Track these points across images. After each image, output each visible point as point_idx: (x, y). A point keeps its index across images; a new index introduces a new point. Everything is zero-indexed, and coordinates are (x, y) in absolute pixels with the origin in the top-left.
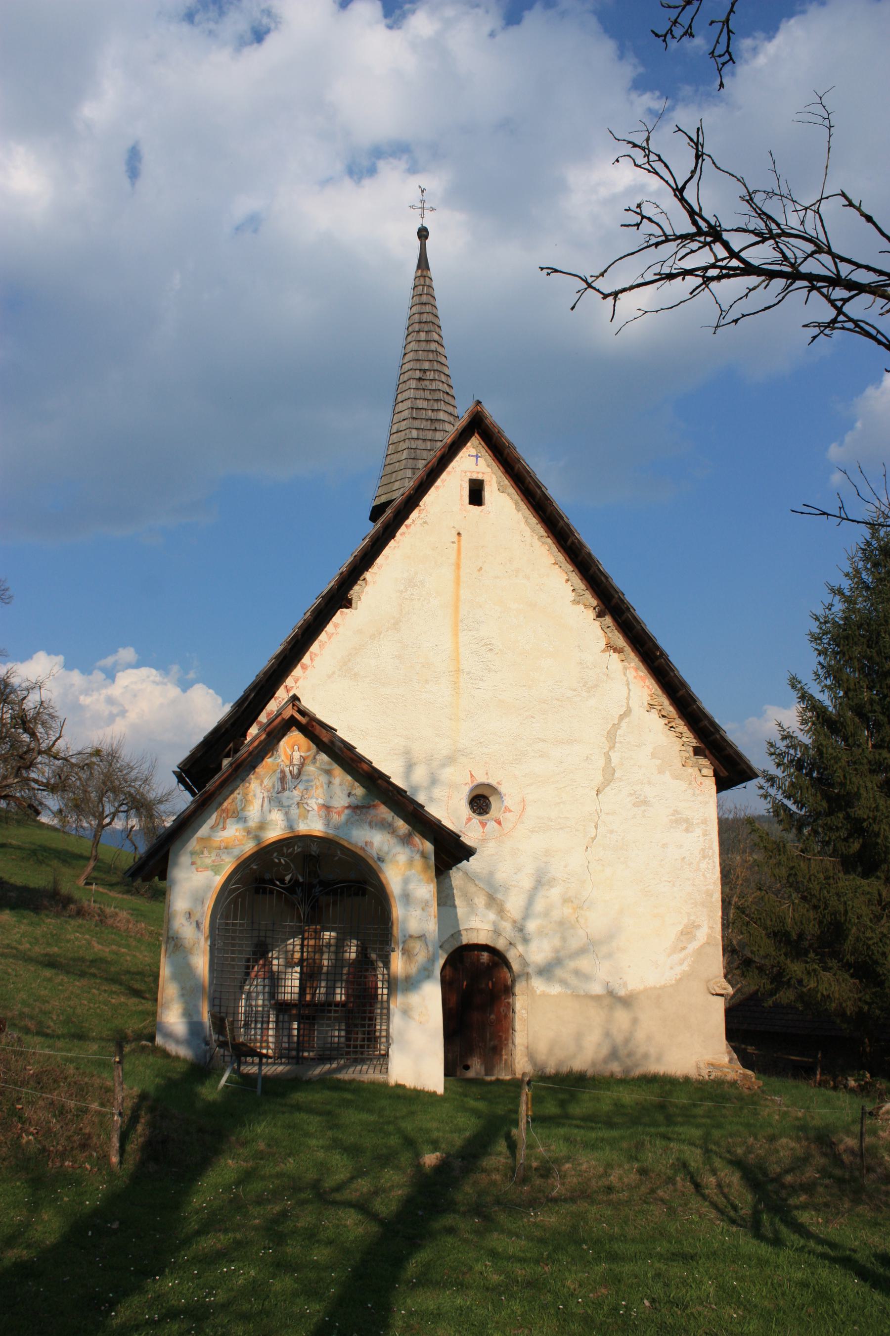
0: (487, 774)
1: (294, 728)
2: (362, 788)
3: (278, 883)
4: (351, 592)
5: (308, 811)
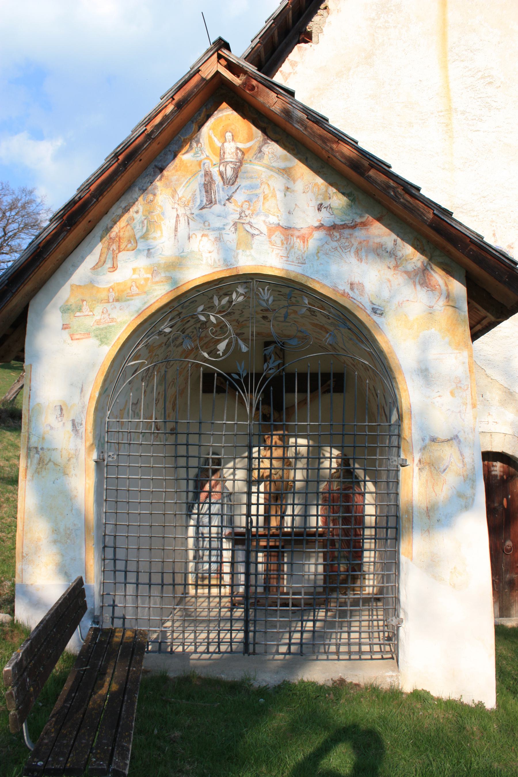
0: (494, 235)
1: (224, 105)
2: (340, 196)
3: (206, 355)
4: (310, 24)
5: (253, 235)
